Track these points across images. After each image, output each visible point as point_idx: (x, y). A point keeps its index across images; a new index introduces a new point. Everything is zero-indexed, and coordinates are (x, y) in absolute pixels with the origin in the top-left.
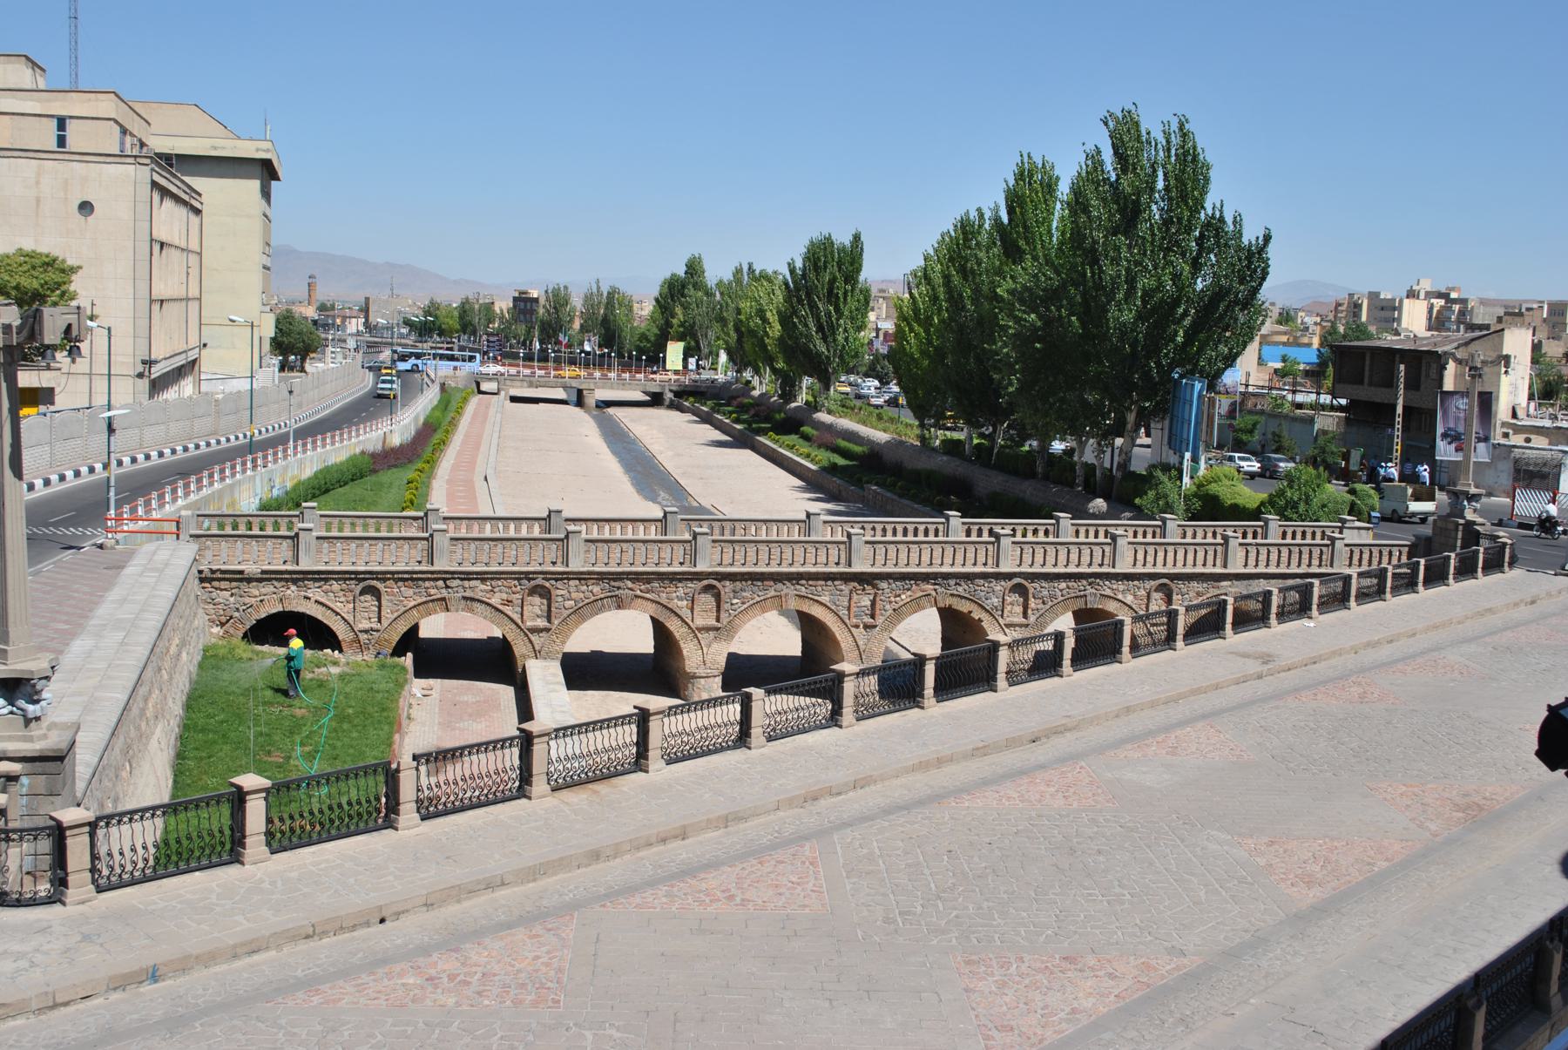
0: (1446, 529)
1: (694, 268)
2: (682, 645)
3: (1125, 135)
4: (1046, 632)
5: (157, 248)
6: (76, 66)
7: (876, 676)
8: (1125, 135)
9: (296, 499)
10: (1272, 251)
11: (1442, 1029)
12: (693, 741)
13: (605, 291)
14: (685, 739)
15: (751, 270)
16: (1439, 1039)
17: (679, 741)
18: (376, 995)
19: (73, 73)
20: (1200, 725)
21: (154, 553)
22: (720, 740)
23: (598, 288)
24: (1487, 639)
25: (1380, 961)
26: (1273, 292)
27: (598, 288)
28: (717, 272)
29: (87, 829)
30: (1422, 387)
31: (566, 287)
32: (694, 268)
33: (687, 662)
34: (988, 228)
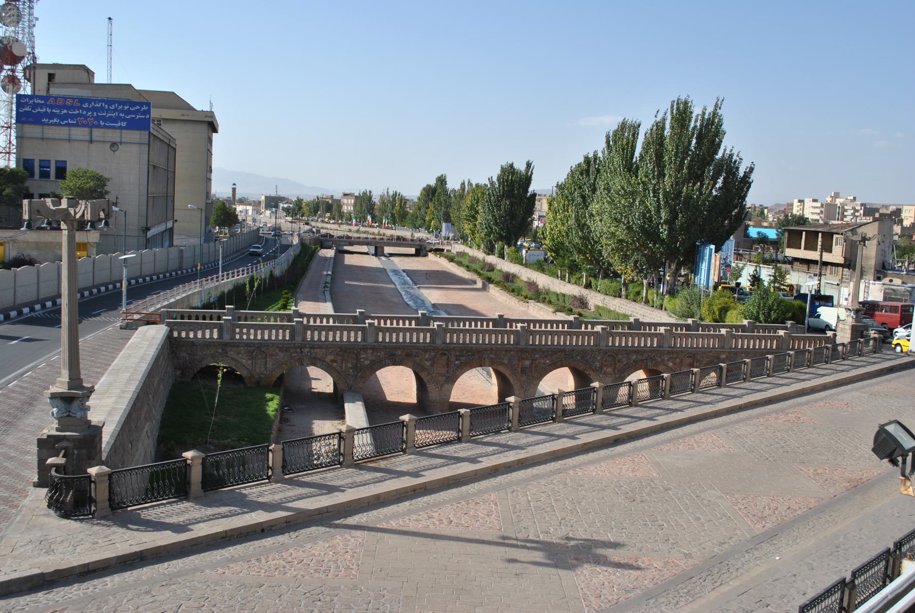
0: (845, 329)
1: (442, 181)
2: (428, 386)
3: (682, 113)
4: (625, 381)
5: (151, 169)
6: (111, 71)
7: (574, 396)
8: (682, 113)
9: (221, 301)
10: (753, 177)
11: (823, 607)
12: (431, 437)
13: (391, 193)
14: (427, 436)
15: (470, 184)
16: (831, 606)
17: (424, 437)
18: (258, 570)
19: (109, 75)
20: (707, 433)
21: (147, 331)
22: (446, 437)
23: (388, 193)
24: (868, 389)
25: (737, 576)
26: (752, 199)
27: (388, 193)
28: (453, 185)
29: (107, 478)
30: (833, 251)
31: (370, 192)
32: (442, 181)
33: (430, 394)
34: (693, 148)
